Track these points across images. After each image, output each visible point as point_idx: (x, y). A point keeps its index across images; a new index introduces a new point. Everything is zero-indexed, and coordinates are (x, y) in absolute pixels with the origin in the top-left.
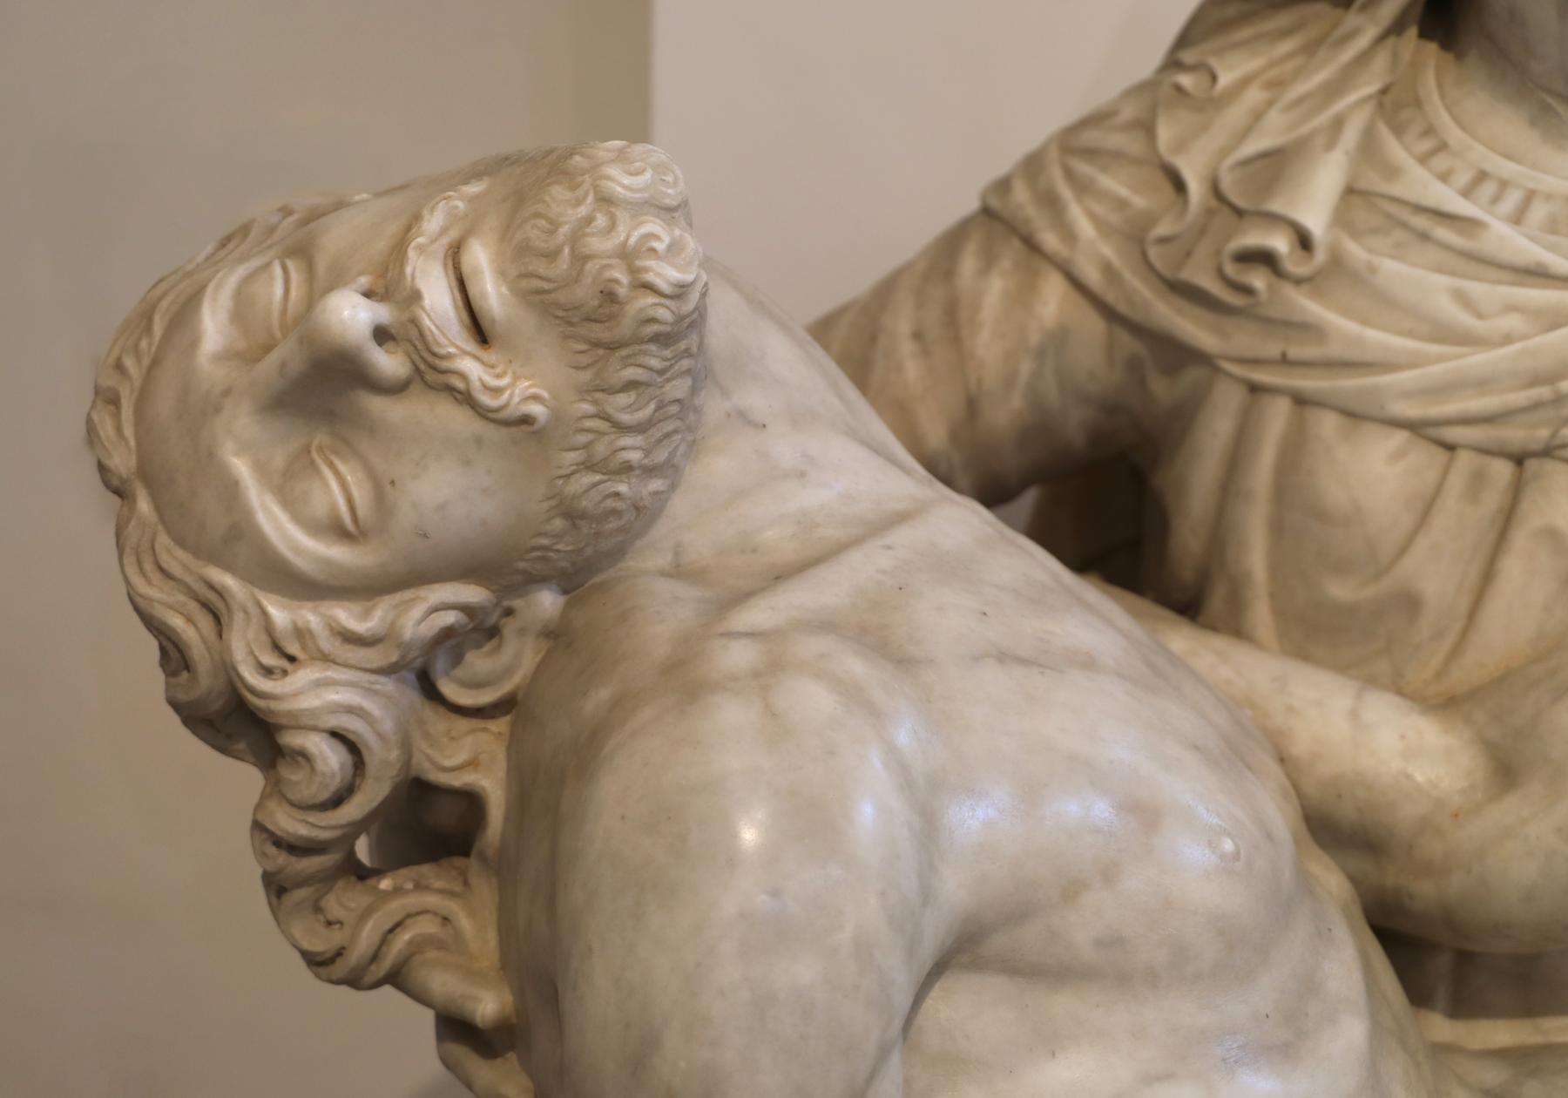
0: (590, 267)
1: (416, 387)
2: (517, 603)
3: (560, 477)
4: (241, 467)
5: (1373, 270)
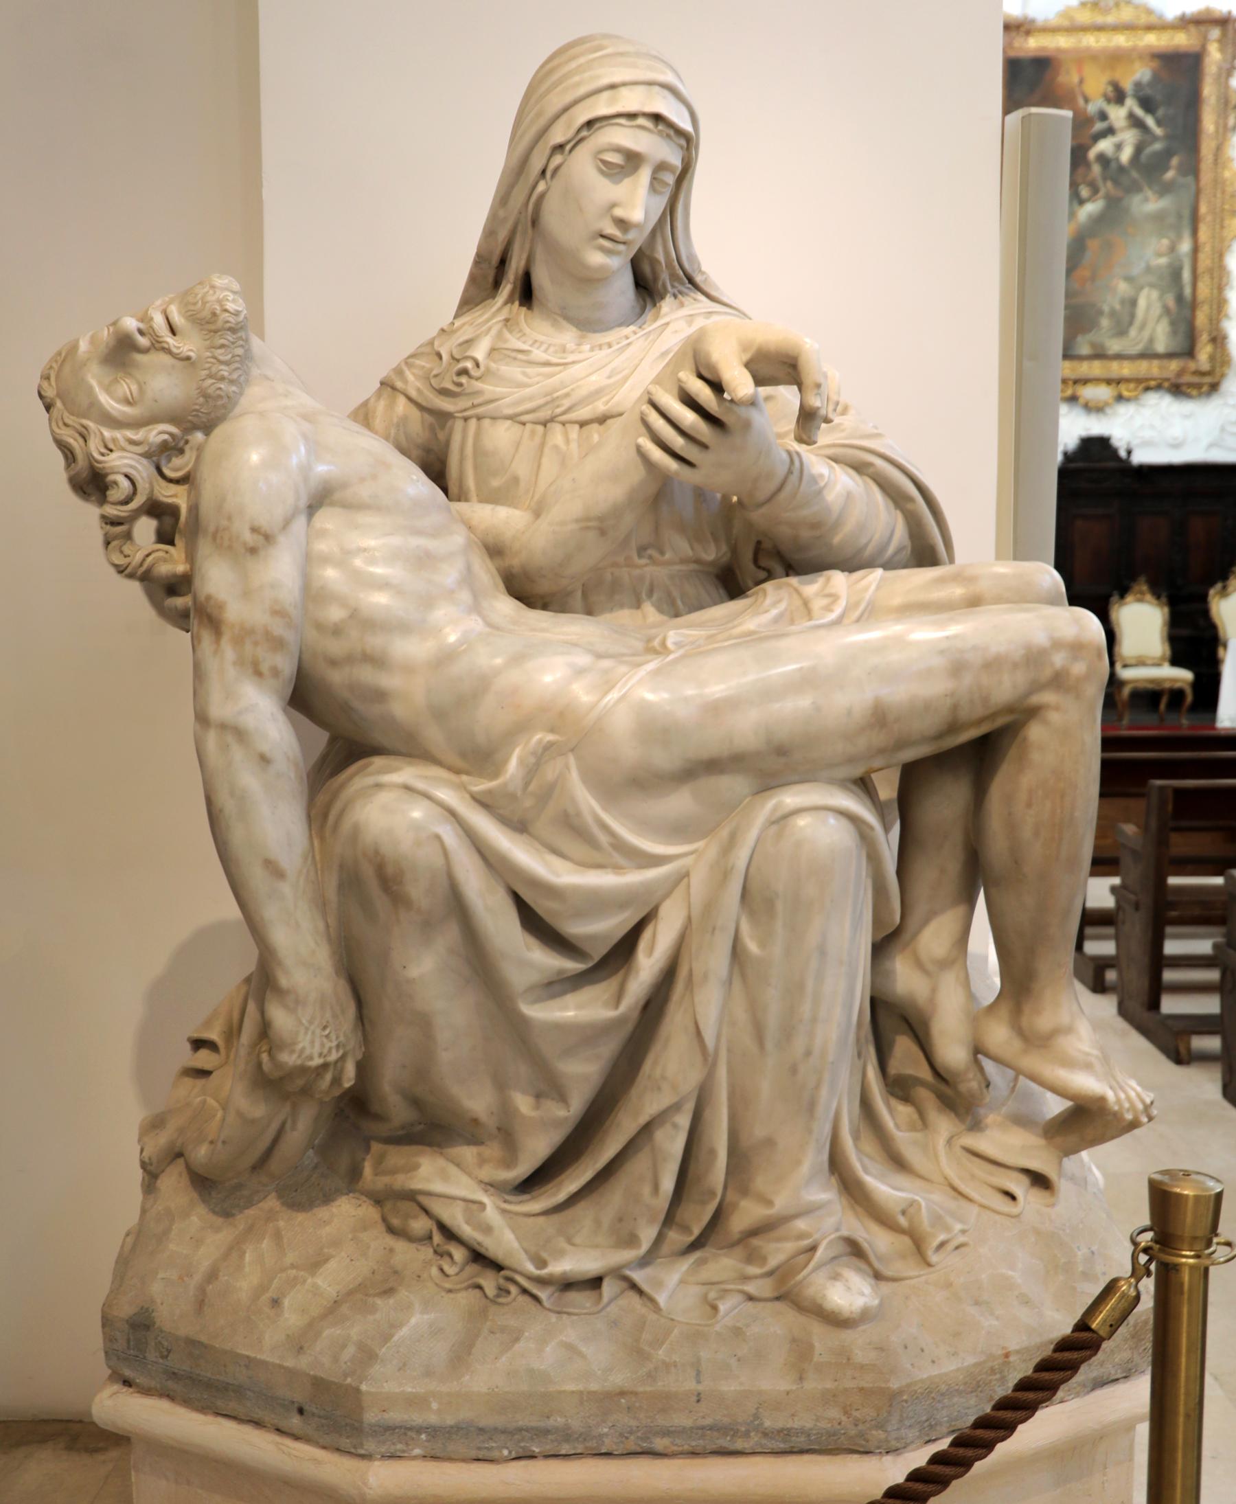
0: (208, 305)
1: (152, 351)
2: (189, 437)
3: (200, 380)
4: (94, 383)
5: (498, 370)
